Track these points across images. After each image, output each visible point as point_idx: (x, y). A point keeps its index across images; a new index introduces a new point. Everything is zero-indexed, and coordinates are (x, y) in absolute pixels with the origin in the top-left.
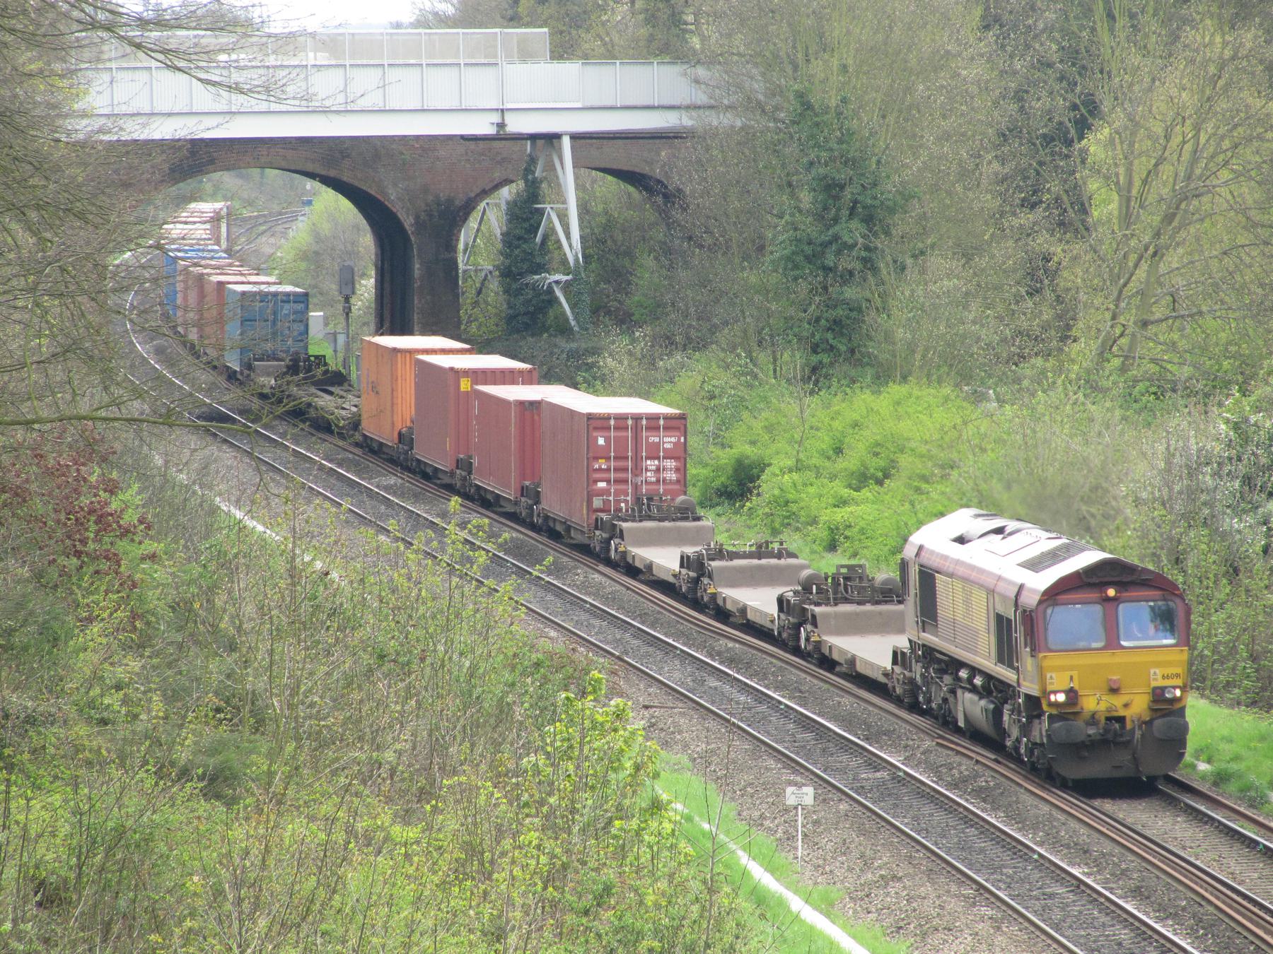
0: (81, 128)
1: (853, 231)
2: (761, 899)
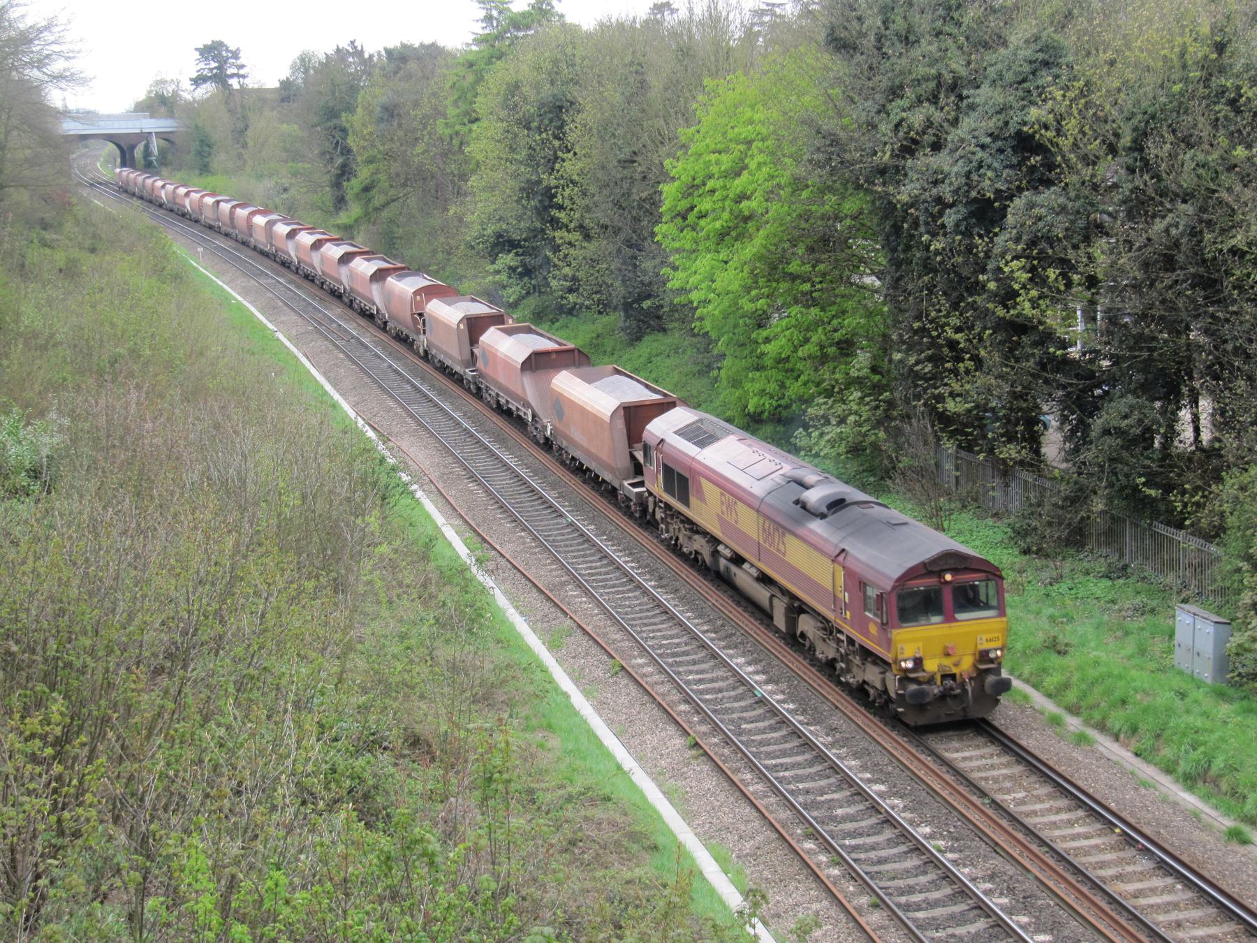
0: (60, 132)
1: (206, 149)
2: (195, 268)
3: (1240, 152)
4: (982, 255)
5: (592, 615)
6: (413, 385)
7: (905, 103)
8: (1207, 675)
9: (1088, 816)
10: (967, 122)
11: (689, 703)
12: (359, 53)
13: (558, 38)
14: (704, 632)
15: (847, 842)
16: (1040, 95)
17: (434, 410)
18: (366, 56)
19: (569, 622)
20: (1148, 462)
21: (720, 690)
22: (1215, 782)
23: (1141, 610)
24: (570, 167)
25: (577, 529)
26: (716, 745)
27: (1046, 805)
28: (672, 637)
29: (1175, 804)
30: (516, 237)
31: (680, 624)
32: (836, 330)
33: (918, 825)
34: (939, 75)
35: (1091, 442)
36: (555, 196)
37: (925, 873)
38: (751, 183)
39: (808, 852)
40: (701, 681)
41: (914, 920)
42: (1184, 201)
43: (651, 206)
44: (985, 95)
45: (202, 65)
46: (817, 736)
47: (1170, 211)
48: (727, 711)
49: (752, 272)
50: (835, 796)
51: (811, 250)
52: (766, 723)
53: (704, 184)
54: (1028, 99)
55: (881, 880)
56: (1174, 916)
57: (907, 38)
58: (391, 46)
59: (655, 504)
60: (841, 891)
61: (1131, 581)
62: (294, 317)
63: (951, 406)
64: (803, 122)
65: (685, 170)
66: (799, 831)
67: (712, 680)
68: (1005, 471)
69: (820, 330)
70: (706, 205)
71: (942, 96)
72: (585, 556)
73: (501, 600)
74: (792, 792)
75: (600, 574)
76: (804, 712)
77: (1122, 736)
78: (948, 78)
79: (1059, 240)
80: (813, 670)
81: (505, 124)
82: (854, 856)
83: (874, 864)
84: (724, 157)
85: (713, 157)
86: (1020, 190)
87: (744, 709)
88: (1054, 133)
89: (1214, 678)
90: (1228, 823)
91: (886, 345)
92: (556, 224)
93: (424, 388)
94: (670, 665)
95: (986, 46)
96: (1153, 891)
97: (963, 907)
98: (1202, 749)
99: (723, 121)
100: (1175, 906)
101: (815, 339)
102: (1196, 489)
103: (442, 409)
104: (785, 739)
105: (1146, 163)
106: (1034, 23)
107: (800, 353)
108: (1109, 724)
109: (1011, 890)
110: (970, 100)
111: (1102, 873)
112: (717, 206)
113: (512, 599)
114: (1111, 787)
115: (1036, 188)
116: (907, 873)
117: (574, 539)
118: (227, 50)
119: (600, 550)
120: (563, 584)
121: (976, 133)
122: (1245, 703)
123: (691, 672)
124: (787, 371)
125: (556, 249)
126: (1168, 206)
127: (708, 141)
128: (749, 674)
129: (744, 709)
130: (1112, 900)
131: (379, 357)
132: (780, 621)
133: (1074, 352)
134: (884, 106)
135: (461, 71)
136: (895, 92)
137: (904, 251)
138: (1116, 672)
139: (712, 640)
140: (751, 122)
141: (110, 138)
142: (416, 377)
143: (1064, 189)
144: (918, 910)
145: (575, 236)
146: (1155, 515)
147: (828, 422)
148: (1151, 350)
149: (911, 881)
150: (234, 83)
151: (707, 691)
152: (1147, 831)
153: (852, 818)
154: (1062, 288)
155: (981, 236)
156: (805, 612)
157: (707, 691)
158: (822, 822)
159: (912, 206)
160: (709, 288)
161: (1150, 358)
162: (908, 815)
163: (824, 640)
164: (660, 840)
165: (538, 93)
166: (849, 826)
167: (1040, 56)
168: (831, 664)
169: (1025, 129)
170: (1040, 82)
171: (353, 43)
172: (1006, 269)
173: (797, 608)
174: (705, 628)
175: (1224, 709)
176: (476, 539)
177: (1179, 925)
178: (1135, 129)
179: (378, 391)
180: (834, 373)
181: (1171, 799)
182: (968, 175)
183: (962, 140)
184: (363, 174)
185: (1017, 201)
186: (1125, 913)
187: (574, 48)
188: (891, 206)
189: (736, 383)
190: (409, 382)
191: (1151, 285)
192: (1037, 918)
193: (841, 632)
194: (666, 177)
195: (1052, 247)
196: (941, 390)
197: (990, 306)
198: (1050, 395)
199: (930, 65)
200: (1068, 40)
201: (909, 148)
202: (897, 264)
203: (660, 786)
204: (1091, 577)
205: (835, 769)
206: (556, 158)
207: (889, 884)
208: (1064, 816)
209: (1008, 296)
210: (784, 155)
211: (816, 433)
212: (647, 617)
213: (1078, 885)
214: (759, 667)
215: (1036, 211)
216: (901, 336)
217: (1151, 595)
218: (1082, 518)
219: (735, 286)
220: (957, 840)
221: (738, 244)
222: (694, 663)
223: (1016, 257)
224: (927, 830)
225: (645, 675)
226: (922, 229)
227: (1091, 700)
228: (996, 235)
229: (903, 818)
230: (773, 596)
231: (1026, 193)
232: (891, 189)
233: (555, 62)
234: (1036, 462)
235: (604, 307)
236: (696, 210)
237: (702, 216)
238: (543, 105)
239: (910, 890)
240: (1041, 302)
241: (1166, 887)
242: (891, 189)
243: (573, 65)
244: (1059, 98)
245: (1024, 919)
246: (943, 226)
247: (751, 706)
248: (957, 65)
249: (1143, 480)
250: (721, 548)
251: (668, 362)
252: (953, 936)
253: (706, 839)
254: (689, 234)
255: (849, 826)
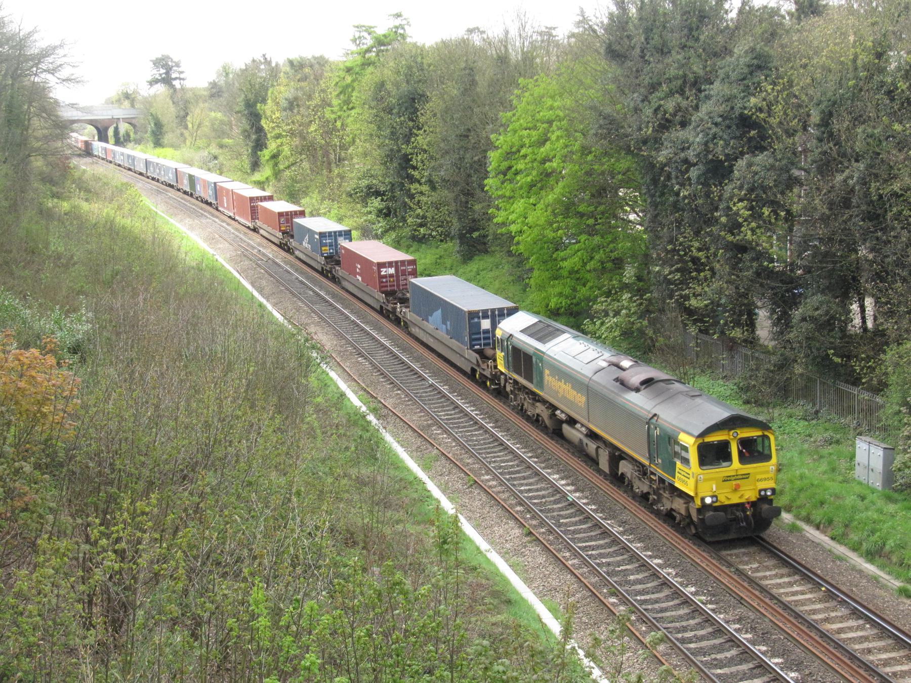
3: (897, 127)
4: (716, 198)
5: (452, 447)
6: (314, 291)
7: (662, 95)
8: (878, 484)
9: (802, 579)
10: (704, 109)
11: (523, 505)
12: (268, 62)
13: (411, 51)
14: (530, 457)
15: (638, 598)
16: (756, 89)
17: (330, 308)
18: (273, 65)
19: (435, 451)
20: (832, 340)
21: (543, 497)
22: (888, 556)
23: (831, 442)
24: (421, 140)
25: (436, 389)
26: (543, 533)
27: (774, 573)
28: (507, 461)
29: (860, 572)
30: (382, 189)
31: (512, 452)
32: (611, 251)
33: (687, 586)
34: (685, 76)
35: (792, 327)
36: (411, 160)
37: (694, 618)
38: (552, 150)
39: (613, 604)
40: (529, 491)
41: (688, 649)
42: (857, 161)
43: (480, 167)
44: (717, 89)
45: (155, 71)
46: (612, 527)
47: (848, 168)
48: (549, 511)
49: (553, 212)
50: (628, 567)
51: (593, 196)
52: (577, 519)
53: (519, 151)
54: (748, 92)
55: (663, 623)
56: (866, 645)
57: (662, 50)
58: (292, 57)
59: (506, 381)
60: (637, 630)
61: (820, 421)
62: (227, 245)
63: (694, 303)
64: (591, 108)
65: (505, 141)
66: (605, 591)
67: (537, 490)
68: (732, 345)
69: (601, 251)
70: (520, 166)
71: (687, 89)
72: (443, 407)
73: (388, 438)
74: (598, 564)
75: (454, 419)
76: (602, 511)
77: (822, 526)
78: (691, 76)
79: (771, 188)
80: (607, 482)
81: (375, 111)
82: (644, 607)
83: (658, 612)
84: (534, 133)
85: (525, 133)
86: (742, 154)
87: (561, 509)
88: (766, 115)
89: (884, 486)
90: (898, 584)
91: (646, 260)
92: (412, 180)
93: (322, 293)
94: (508, 480)
95: (716, 55)
96: (850, 629)
97: (721, 640)
98: (878, 534)
99: (531, 108)
100: (866, 639)
101: (597, 257)
102: (868, 358)
103: (335, 308)
104: (590, 529)
105: (831, 134)
106: (750, 39)
107: (588, 268)
108: (812, 517)
109: (753, 629)
110: (707, 93)
111: (815, 617)
112: (528, 166)
113: (395, 436)
114: (817, 560)
115: (753, 152)
116: (680, 618)
117: (434, 395)
118: (172, 61)
119: (453, 403)
120: (429, 426)
121: (712, 115)
122: (905, 503)
123: (522, 485)
124: (578, 279)
125: (412, 197)
126: (846, 164)
127: (522, 121)
128: (562, 485)
129: (561, 509)
130: (823, 635)
131: (289, 272)
132: (604, 464)
133: (778, 266)
134: (646, 97)
135: (342, 74)
136: (654, 87)
137: (660, 197)
138: (816, 483)
139: (535, 463)
140: (551, 108)
141: (92, 122)
142: (315, 285)
143: (773, 153)
144: (690, 643)
145: (425, 188)
146: (837, 376)
147: (607, 315)
148: (835, 263)
149: (684, 624)
150: (177, 83)
151: (535, 497)
152: (844, 589)
153: (640, 582)
154: (773, 221)
155: (716, 186)
156: (624, 459)
157: (535, 497)
158: (620, 585)
159: (665, 165)
160: (523, 222)
161: (833, 270)
162: (679, 579)
163: (640, 479)
164: (513, 597)
165: (398, 89)
166: (639, 587)
167: (755, 62)
168: (645, 497)
169: (746, 112)
170: (756, 80)
171: (264, 55)
172: (735, 208)
173: (617, 456)
174: (530, 455)
175: (891, 508)
176: (366, 395)
177: (869, 651)
178: (823, 112)
179: (290, 296)
180: (611, 280)
181: (858, 568)
182: (706, 144)
183: (702, 120)
184: (272, 146)
185: (740, 162)
186: (832, 644)
187: (422, 58)
188: (653, 166)
189: (541, 287)
190: (311, 289)
191: (836, 219)
192: (773, 647)
193: (655, 475)
194: (491, 146)
195: (765, 193)
196: (687, 292)
197: (723, 233)
198: (763, 295)
199: (678, 69)
200: (774, 51)
201: (665, 125)
202: (655, 205)
203: (506, 561)
204: (793, 419)
205: (626, 549)
206: (411, 134)
207: (669, 625)
208: (786, 580)
209: (734, 227)
210: (576, 131)
211: (598, 323)
212: (489, 448)
213: (800, 625)
214: (569, 481)
215: (754, 168)
216: (658, 255)
217: (836, 431)
218: (787, 379)
219: (542, 221)
220: (714, 596)
221: (543, 193)
222: (524, 478)
223: (741, 200)
224: (693, 589)
225: (490, 487)
226: (674, 181)
227: (798, 503)
228: (726, 184)
229: (676, 581)
230: (598, 447)
231: (746, 156)
232: (653, 153)
233: (410, 68)
234: (752, 342)
235: (446, 237)
236: (513, 169)
237: (517, 173)
238: (401, 98)
239: (684, 629)
240: (758, 231)
241: (858, 626)
242: (653, 153)
243: (422, 70)
244: (769, 91)
245: (764, 648)
246: (689, 179)
247: (565, 507)
248: (697, 68)
249: (832, 351)
250: (558, 412)
251: (491, 274)
252: (715, 659)
253: (541, 596)
254: (508, 186)
255: (639, 587)
